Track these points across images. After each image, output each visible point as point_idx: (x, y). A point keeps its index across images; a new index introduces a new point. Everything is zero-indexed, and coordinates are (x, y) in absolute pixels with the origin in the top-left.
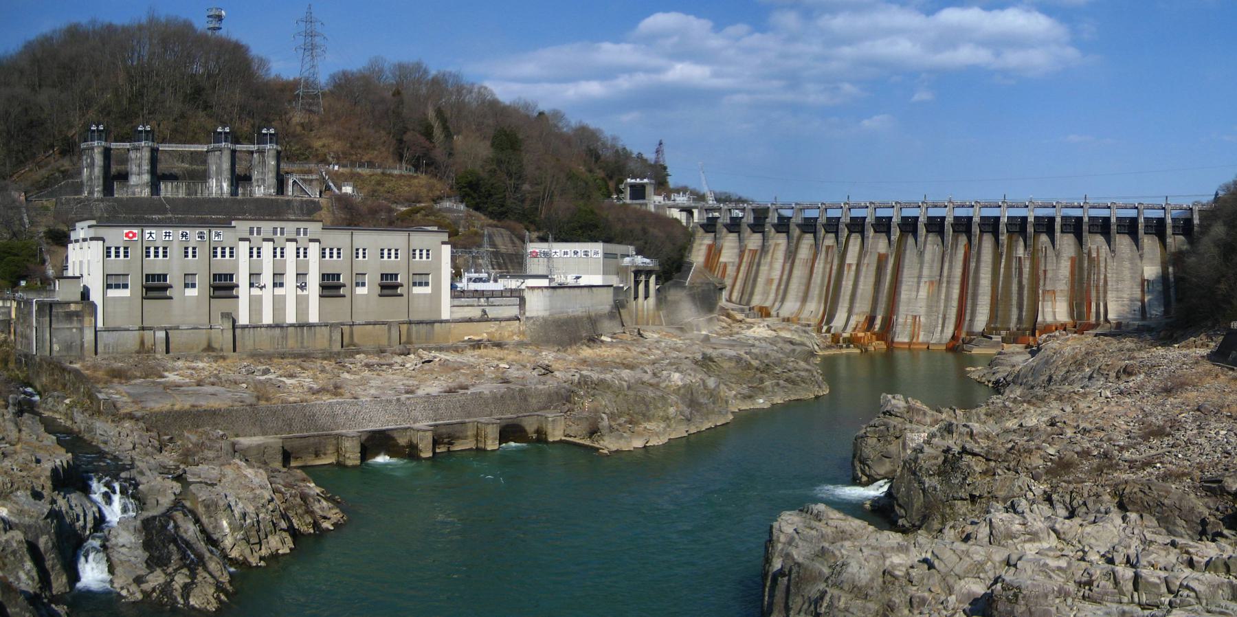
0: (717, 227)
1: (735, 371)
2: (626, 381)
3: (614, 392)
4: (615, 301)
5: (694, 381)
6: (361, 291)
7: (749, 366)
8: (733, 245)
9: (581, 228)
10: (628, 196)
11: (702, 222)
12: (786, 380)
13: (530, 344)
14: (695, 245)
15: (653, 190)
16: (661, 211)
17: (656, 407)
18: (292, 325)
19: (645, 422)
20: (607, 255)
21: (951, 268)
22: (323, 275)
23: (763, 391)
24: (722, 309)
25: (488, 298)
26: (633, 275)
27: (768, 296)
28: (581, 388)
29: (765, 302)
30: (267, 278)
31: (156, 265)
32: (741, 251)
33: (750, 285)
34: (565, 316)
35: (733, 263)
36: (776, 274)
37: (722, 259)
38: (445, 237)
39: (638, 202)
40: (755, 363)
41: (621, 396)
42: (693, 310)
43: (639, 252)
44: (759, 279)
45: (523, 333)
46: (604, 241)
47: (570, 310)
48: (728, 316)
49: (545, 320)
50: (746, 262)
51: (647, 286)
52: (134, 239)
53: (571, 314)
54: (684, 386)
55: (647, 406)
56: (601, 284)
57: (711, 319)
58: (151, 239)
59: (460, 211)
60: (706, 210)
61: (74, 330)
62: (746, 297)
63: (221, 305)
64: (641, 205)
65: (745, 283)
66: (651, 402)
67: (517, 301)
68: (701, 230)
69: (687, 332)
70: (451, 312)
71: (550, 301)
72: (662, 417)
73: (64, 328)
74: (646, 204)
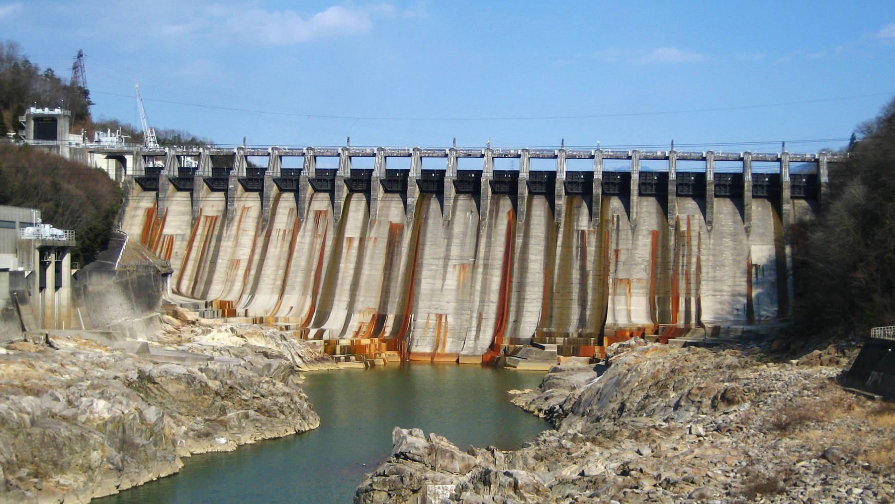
0: (160, 183)
1: (186, 397)
2: (28, 413)
4: (11, 293)
7: (205, 388)
8: (182, 209)
12: (258, 410)
14: (127, 209)
16: (78, 158)
17: (73, 452)
24: (167, 304)
26: (37, 253)
33: (207, 269)
35: (183, 236)
37: (167, 231)
40: (214, 385)
41: (21, 436)
42: (126, 305)
44: (220, 261)
48: (176, 315)
50: (202, 235)
51: (58, 270)
54: (113, 419)
55: (60, 451)
62: (201, 287)
64: (50, 147)
66: (64, 445)
68: (137, 187)
69: (116, 339)
72: (82, 466)
74: (58, 147)
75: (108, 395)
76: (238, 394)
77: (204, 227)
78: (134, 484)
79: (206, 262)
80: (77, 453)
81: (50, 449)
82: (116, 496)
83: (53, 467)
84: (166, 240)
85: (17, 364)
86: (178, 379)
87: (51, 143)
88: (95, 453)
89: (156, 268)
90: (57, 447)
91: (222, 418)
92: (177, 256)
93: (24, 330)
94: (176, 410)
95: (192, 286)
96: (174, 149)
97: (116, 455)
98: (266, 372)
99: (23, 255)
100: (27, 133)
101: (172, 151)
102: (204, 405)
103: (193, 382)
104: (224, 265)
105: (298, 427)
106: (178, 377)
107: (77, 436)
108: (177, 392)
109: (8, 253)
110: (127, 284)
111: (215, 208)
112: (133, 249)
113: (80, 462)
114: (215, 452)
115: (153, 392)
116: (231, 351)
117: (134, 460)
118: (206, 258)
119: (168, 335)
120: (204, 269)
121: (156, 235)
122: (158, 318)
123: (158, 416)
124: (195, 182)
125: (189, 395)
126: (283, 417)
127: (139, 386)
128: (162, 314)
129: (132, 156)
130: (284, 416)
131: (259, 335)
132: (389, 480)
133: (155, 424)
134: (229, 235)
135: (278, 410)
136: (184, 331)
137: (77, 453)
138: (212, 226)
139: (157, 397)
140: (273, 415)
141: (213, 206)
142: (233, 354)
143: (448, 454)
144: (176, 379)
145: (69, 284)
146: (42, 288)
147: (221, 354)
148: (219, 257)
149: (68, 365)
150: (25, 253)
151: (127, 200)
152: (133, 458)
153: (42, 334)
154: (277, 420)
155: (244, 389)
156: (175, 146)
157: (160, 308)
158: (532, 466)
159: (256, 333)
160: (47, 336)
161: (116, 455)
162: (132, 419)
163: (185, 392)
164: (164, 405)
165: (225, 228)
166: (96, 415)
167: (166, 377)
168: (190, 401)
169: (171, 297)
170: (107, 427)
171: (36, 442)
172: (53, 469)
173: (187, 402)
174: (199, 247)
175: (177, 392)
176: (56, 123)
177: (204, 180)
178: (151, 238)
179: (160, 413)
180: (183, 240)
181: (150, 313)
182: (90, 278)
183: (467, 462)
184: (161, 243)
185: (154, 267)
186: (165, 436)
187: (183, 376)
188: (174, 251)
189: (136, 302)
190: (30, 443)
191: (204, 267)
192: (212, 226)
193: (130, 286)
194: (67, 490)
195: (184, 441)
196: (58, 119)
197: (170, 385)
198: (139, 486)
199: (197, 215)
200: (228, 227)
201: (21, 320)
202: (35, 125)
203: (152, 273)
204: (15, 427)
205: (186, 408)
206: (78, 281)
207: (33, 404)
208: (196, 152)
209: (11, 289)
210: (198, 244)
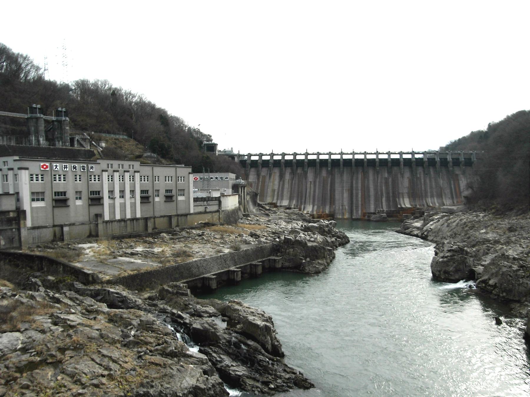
6: (157, 199)
18: (129, 219)
21: (357, 183)
22: (141, 191)
25: (207, 201)
29: (273, 200)
30: (117, 194)
31: (60, 185)
35: (255, 182)
36: (276, 187)
38: (190, 170)
52: (47, 169)
58: (56, 169)
61: (14, 230)
63: (95, 210)
70: (194, 209)
73: (6, 230)
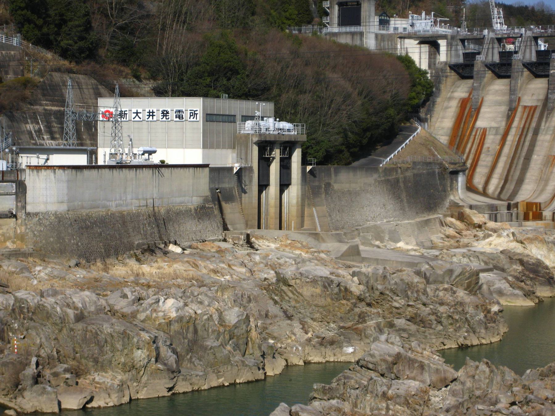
0: (475, 69)
1: (322, 302)
2: (76, 308)
3: (55, 324)
4: (212, 190)
5: (199, 312)
7: (345, 292)
8: (498, 98)
9: (211, 74)
10: (336, 20)
11: (454, 61)
12: (411, 320)
13: (31, 255)
14: (439, 100)
15: (373, 9)
16: (386, 45)
17: (114, 350)
19: (96, 371)
20: (209, 117)
23: (361, 334)
24: (455, 205)
26: (256, 149)
27: (546, 185)
28: (15, 319)
32: (510, 110)
33: (520, 167)
34: (102, 212)
35: (497, 129)
37: (481, 123)
39: (348, 29)
40: (356, 288)
41: (65, 331)
42: (390, 206)
43: (279, 115)
44: (535, 157)
45: (22, 237)
46: (205, 95)
47: (113, 204)
48: (461, 217)
49: (59, 218)
50: (517, 128)
51: (285, 166)
53: (114, 209)
54: (180, 319)
55: (101, 348)
56: (200, 162)
57: (427, 222)
59: (11, 47)
60: (463, 41)
62: (511, 187)
64: (353, 34)
65: (512, 163)
66: (106, 341)
67: (12, 188)
68: (453, 75)
69: (324, 241)
71: (69, 188)
72: (124, 365)
74: (361, 34)
75: (189, 294)
76: (389, 301)
77: (521, 118)
78: (196, 388)
79: (519, 158)
80: (118, 351)
81: (92, 345)
82: (166, 399)
83: (93, 364)
84: (478, 134)
85: (180, 263)
86: (314, 281)
87: (353, 29)
88: (140, 352)
89: (444, 165)
90: (98, 343)
91: (360, 326)
92: (489, 151)
93: (225, 228)
94: (309, 315)
95: (501, 186)
96: (530, 29)
97: (171, 356)
98: (447, 279)
99: (241, 150)
100: (331, 19)
101: (491, 33)
102: (341, 311)
103: (329, 285)
104: (539, 162)
105: (461, 341)
106: (314, 280)
107: (118, 333)
108: (312, 296)
109: (224, 147)
110: (398, 181)
111: (535, 97)
112: (421, 144)
113: (123, 360)
114: (337, 362)
115: (287, 295)
116: (481, 257)
117: (201, 363)
118: (520, 154)
119: (447, 239)
120: (516, 167)
121: (468, 129)
122: (437, 220)
123: (240, 318)
124: (513, 67)
125: (325, 299)
126: (440, 328)
127: (275, 289)
128: (445, 216)
129: (446, 41)
130: (442, 327)
131: (541, 241)
132: (329, 388)
133: (236, 326)
134: (548, 127)
135: (436, 320)
136: (466, 236)
137: (118, 351)
138: (530, 117)
139: (291, 300)
140: (428, 325)
141: (533, 94)
142: (483, 261)
143: (416, 365)
144: (311, 282)
145: (300, 181)
146: (263, 186)
147: (470, 260)
148: (535, 152)
149: (235, 265)
150: (243, 148)
151: (439, 89)
152: (200, 360)
153: (241, 234)
154: (431, 331)
155: (398, 296)
156: (532, 27)
157: (445, 209)
158: (509, 383)
159: (536, 239)
160: (248, 236)
161: (171, 356)
162: (206, 320)
163: (321, 296)
164: (297, 309)
165: (544, 119)
166: (161, 314)
167: (301, 280)
168: (326, 306)
169: (462, 197)
170: (172, 327)
171: (78, 337)
172: (94, 366)
173: (323, 307)
174: (513, 141)
175: (312, 296)
176: (361, 7)
177: (524, 65)
178: (462, 131)
179: (242, 315)
180: (496, 134)
181: (428, 215)
182: (336, 176)
183: (443, 375)
184: (472, 137)
185: (441, 165)
186: (251, 339)
187: (320, 279)
188: (486, 146)
189: (408, 202)
190: (72, 338)
191: (517, 164)
192: (530, 117)
193: (402, 185)
194: (100, 388)
195: (300, 348)
196: (362, 3)
197: (305, 289)
198: (201, 390)
199: (514, 105)
200: (547, 118)
201: (223, 219)
202: (339, 10)
203: (437, 171)
204: (58, 321)
205: (321, 314)
206: (317, 179)
207: (87, 299)
208: (517, 33)
209: (212, 186)
210: (512, 138)
